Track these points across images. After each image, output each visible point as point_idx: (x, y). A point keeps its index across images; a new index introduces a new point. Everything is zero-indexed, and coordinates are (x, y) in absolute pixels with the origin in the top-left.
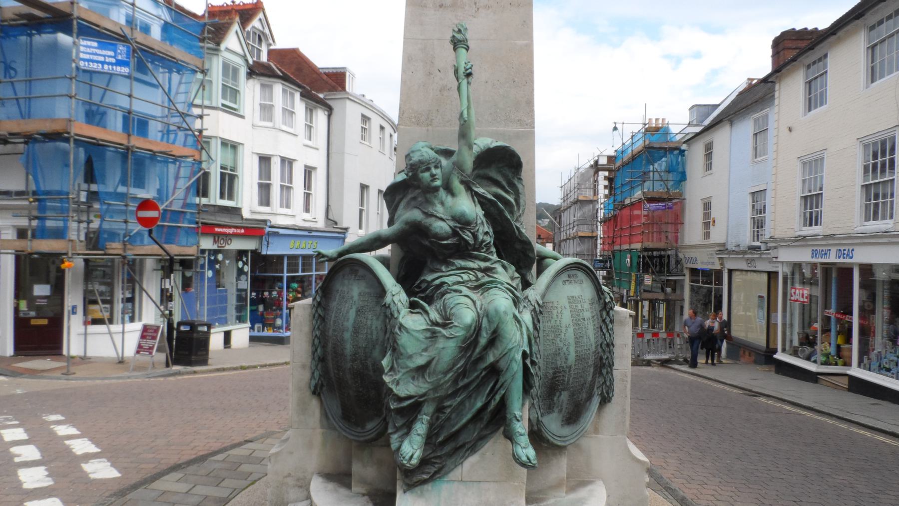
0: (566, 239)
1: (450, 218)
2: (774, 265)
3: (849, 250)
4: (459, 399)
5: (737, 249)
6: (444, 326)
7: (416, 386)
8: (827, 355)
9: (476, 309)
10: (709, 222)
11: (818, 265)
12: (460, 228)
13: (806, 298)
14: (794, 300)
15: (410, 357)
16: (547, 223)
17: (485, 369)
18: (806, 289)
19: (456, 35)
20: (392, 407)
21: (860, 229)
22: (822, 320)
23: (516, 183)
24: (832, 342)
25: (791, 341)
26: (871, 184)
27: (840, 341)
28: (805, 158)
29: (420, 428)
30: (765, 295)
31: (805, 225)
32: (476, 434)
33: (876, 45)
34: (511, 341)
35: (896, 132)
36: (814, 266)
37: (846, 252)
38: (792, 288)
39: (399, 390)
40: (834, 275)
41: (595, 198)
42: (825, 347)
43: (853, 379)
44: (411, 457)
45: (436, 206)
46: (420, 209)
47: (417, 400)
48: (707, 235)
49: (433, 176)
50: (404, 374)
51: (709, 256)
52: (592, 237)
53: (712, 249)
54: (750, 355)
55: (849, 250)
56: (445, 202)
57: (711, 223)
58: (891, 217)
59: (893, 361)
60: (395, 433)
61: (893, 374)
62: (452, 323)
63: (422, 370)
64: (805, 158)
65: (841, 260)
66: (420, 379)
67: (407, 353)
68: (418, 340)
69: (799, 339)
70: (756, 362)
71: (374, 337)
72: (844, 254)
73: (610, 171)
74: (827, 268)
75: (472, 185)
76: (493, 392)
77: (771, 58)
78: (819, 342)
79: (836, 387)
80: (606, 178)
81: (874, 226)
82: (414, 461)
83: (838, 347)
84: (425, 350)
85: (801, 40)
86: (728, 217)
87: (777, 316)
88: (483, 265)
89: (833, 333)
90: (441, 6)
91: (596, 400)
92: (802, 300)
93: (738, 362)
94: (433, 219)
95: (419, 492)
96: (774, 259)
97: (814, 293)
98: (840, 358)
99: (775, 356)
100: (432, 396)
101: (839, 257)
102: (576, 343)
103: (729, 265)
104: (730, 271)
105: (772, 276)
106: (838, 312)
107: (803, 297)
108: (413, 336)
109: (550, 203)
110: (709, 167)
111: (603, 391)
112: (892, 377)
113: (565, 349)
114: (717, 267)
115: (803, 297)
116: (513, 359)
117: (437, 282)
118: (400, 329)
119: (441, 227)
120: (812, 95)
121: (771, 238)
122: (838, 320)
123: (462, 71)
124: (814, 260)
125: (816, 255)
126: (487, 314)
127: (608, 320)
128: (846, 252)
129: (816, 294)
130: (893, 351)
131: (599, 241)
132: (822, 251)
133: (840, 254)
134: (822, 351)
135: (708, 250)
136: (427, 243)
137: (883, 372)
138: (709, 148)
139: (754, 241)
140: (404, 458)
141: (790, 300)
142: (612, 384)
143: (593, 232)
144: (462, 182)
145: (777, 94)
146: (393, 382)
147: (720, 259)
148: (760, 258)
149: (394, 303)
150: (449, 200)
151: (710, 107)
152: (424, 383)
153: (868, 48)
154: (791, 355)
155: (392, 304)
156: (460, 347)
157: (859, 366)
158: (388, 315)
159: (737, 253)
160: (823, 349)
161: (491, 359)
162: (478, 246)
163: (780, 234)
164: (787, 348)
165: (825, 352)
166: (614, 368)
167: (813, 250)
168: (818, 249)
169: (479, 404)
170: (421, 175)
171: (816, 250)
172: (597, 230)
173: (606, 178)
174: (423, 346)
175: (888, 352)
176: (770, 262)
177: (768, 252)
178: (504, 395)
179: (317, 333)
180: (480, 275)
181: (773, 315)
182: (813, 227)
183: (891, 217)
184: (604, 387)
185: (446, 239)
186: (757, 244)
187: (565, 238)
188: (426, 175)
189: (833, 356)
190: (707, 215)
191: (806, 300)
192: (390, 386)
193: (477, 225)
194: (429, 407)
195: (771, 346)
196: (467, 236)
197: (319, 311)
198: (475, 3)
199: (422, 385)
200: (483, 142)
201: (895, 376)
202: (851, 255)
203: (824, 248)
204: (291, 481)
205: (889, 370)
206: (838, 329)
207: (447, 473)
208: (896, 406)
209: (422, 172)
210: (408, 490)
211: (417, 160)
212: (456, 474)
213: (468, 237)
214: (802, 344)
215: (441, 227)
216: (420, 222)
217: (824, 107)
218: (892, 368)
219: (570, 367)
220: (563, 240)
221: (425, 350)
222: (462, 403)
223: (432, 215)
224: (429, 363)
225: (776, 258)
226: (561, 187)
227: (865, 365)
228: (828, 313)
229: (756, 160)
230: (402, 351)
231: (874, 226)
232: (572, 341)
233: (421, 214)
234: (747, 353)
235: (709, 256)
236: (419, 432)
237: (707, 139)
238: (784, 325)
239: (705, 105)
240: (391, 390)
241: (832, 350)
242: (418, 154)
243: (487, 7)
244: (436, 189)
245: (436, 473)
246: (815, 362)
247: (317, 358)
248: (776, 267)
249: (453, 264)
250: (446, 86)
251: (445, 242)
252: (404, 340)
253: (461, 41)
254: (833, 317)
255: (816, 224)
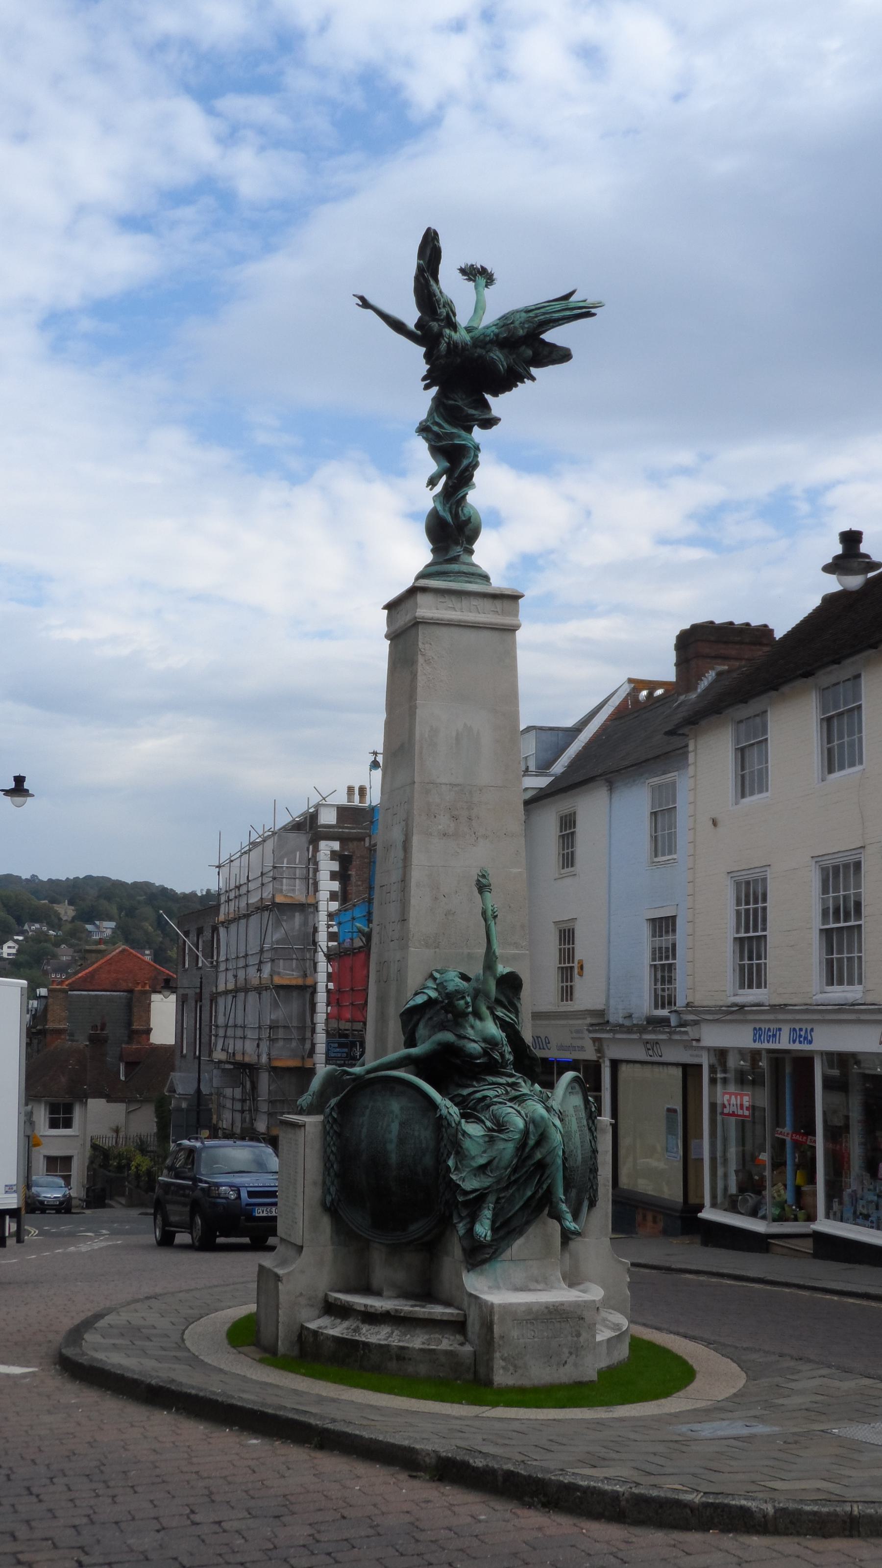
0: (236, 991)
1: (481, 1040)
2: (695, 1053)
3: (806, 1029)
4: (511, 1191)
5: (627, 1023)
6: (500, 1131)
7: (479, 1182)
8: (782, 1205)
9: (523, 1117)
10: (572, 968)
11: (764, 1053)
12: (490, 1049)
13: (748, 1109)
14: (728, 1115)
15: (473, 1158)
16: (109, 932)
17: (533, 1165)
18: (746, 1095)
19: (480, 879)
20: (460, 1200)
21: (820, 998)
22: (773, 1147)
23: (516, 1002)
24: (789, 1183)
25: (726, 1189)
26: (832, 929)
27: (799, 1181)
28: (739, 874)
29: (487, 1214)
30: (679, 1108)
31: (742, 986)
32: (524, 1219)
33: (832, 717)
34: (554, 1140)
35: (862, 856)
36: (755, 1055)
37: (803, 1033)
38: (725, 1093)
39: (465, 1186)
40: (788, 1070)
41: (311, 901)
42: (779, 1191)
43: (818, 1237)
44: (486, 1236)
45: (467, 1029)
46: (450, 1031)
47: (482, 1193)
48: (567, 993)
49: (467, 1003)
50: (468, 1172)
51: (574, 1035)
52: (301, 988)
53: (580, 1022)
54: (655, 1221)
55: (806, 1029)
56: (475, 1026)
57: (576, 971)
58: (860, 983)
59: (872, 1202)
60: (459, 1222)
61: (872, 1222)
62: (508, 1129)
63: (482, 1169)
64: (739, 874)
65: (797, 1046)
66: (482, 1175)
67: (471, 1154)
68: (479, 1144)
69: (737, 1180)
70: (666, 1232)
71: (424, 1145)
72: (800, 1036)
73: (343, 840)
74: (778, 1058)
75: (494, 1010)
76: (540, 1183)
77: (675, 668)
78: (768, 1183)
79: (797, 1253)
80: (334, 855)
81: (840, 993)
82: (488, 1238)
83: (798, 1191)
84: (484, 1152)
85: (726, 643)
86: (609, 962)
87: (701, 1147)
88: (510, 1080)
89: (789, 1168)
90: (444, 835)
91: (586, 1203)
92: (740, 1112)
93: (634, 1236)
94: (466, 1041)
95: (479, 1271)
96: (694, 1043)
97: (759, 1104)
98: (801, 1208)
99: (700, 1215)
100: (495, 1188)
101: (794, 1042)
102: (581, 1146)
103: (614, 1052)
104: (615, 1064)
105: (690, 1072)
106: (796, 1131)
107: (742, 1108)
108: (475, 1141)
109: (114, 877)
110: (568, 860)
111: (590, 1194)
112: (872, 1227)
113: (575, 1151)
114: (590, 1054)
115: (742, 1108)
116: (557, 1154)
117: (478, 1095)
118: (463, 1136)
119: (475, 1047)
120: (747, 771)
121: (688, 1005)
122: (797, 1145)
123: (489, 913)
124: (757, 1045)
125: (760, 1036)
126: (533, 1121)
127: (593, 1129)
128: (803, 1033)
129: (762, 1106)
130: (871, 1187)
131: (321, 997)
132: (769, 1030)
133: (796, 1035)
134: (774, 1198)
135: (571, 1022)
136: (458, 1061)
137: (859, 1221)
138: (568, 823)
139: (656, 1007)
140: (480, 1237)
141: (722, 1113)
142: (597, 1190)
143: (305, 976)
144: (488, 1008)
145: (691, 758)
146: (460, 1179)
147: (594, 1040)
148: (670, 1039)
149: (450, 1114)
150: (478, 1023)
151: (561, 734)
152: (487, 1178)
153: (822, 719)
154: (725, 1210)
155: (448, 1116)
156: (517, 1147)
157: (827, 1216)
158: (440, 1123)
159: (629, 1030)
160: (775, 1195)
161: (538, 1156)
162: (504, 1064)
163: (701, 998)
164: (719, 1199)
165: (778, 1199)
166: (599, 1174)
167: (755, 1029)
168: (763, 1026)
169: (529, 1193)
170: (457, 1003)
171: (760, 1029)
172: (315, 971)
173: (334, 855)
174: (483, 1149)
175: (865, 1190)
176: (685, 1047)
177: (683, 1029)
178: (549, 1187)
179: (333, 1149)
180: (509, 1089)
181: (693, 1143)
182: (755, 991)
183: (860, 983)
184: (591, 1190)
185: (479, 1058)
186: (664, 1013)
187: (231, 986)
188: (462, 1002)
189: (790, 1206)
190: (567, 954)
191: (747, 1113)
192: (458, 1182)
193: (503, 1046)
194: (492, 1198)
195: (692, 1200)
196: (496, 1055)
197: (335, 1127)
198: (475, 833)
199: (486, 1180)
200: (502, 969)
201: (874, 1225)
202: (809, 1038)
203: (773, 1026)
204: (303, 1301)
205: (866, 1217)
206: (797, 1160)
207: (501, 1253)
208: (879, 1269)
209: (458, 1000)
210: (472, 1269)
211: (454, 990)
212: (507, 1254)
213: (497, 1056)
214: (742, 1189)
215: (474, 1048)
216: (453, 1043)
217: (764, 795)
218: (871, 1212)
219: (578, 1167)
220: (226, 992)
221: (484, 1152)
222: (512, 1195)
223: (465, 1038)
224: (489, 1163)
225: (698, 1040)
226: (219, 867)
227: (835, 1214)
228: (781, 1133)
229: (656, 860)
230: (467, 1153)
231: (840, 993)
232: (578, 1144)
233: (454, 1036)
234: (650, 1217)
235: (574, 1035)
236: (488, 1217)
237: (563, 805)
238: (713, 1160)
239: (551, 729)
240: (459, 1186)
241: (788, 1196)
242: (452, 983)
243: (486, 837)
244: (467, 1014)
245: (494, 1253)
246: (764, 1218)
247: (332, 1174)
248: (697, 1056)
249: (485, 1080)
250: (451, 910)
251: (478, 1061)
252: (467, 1144)
253: (486, 886)
254: (788, 1139)
255: (759, 986)
